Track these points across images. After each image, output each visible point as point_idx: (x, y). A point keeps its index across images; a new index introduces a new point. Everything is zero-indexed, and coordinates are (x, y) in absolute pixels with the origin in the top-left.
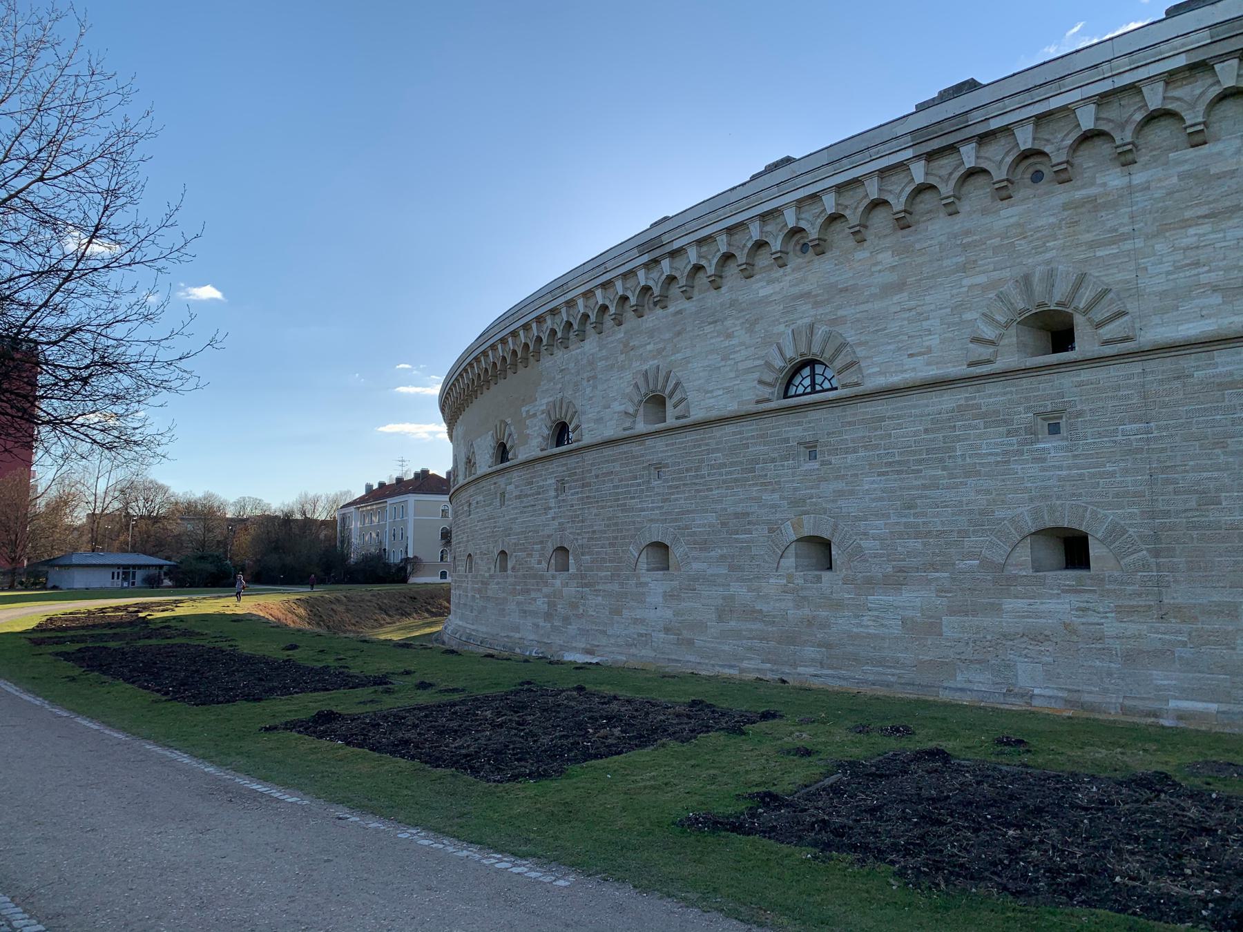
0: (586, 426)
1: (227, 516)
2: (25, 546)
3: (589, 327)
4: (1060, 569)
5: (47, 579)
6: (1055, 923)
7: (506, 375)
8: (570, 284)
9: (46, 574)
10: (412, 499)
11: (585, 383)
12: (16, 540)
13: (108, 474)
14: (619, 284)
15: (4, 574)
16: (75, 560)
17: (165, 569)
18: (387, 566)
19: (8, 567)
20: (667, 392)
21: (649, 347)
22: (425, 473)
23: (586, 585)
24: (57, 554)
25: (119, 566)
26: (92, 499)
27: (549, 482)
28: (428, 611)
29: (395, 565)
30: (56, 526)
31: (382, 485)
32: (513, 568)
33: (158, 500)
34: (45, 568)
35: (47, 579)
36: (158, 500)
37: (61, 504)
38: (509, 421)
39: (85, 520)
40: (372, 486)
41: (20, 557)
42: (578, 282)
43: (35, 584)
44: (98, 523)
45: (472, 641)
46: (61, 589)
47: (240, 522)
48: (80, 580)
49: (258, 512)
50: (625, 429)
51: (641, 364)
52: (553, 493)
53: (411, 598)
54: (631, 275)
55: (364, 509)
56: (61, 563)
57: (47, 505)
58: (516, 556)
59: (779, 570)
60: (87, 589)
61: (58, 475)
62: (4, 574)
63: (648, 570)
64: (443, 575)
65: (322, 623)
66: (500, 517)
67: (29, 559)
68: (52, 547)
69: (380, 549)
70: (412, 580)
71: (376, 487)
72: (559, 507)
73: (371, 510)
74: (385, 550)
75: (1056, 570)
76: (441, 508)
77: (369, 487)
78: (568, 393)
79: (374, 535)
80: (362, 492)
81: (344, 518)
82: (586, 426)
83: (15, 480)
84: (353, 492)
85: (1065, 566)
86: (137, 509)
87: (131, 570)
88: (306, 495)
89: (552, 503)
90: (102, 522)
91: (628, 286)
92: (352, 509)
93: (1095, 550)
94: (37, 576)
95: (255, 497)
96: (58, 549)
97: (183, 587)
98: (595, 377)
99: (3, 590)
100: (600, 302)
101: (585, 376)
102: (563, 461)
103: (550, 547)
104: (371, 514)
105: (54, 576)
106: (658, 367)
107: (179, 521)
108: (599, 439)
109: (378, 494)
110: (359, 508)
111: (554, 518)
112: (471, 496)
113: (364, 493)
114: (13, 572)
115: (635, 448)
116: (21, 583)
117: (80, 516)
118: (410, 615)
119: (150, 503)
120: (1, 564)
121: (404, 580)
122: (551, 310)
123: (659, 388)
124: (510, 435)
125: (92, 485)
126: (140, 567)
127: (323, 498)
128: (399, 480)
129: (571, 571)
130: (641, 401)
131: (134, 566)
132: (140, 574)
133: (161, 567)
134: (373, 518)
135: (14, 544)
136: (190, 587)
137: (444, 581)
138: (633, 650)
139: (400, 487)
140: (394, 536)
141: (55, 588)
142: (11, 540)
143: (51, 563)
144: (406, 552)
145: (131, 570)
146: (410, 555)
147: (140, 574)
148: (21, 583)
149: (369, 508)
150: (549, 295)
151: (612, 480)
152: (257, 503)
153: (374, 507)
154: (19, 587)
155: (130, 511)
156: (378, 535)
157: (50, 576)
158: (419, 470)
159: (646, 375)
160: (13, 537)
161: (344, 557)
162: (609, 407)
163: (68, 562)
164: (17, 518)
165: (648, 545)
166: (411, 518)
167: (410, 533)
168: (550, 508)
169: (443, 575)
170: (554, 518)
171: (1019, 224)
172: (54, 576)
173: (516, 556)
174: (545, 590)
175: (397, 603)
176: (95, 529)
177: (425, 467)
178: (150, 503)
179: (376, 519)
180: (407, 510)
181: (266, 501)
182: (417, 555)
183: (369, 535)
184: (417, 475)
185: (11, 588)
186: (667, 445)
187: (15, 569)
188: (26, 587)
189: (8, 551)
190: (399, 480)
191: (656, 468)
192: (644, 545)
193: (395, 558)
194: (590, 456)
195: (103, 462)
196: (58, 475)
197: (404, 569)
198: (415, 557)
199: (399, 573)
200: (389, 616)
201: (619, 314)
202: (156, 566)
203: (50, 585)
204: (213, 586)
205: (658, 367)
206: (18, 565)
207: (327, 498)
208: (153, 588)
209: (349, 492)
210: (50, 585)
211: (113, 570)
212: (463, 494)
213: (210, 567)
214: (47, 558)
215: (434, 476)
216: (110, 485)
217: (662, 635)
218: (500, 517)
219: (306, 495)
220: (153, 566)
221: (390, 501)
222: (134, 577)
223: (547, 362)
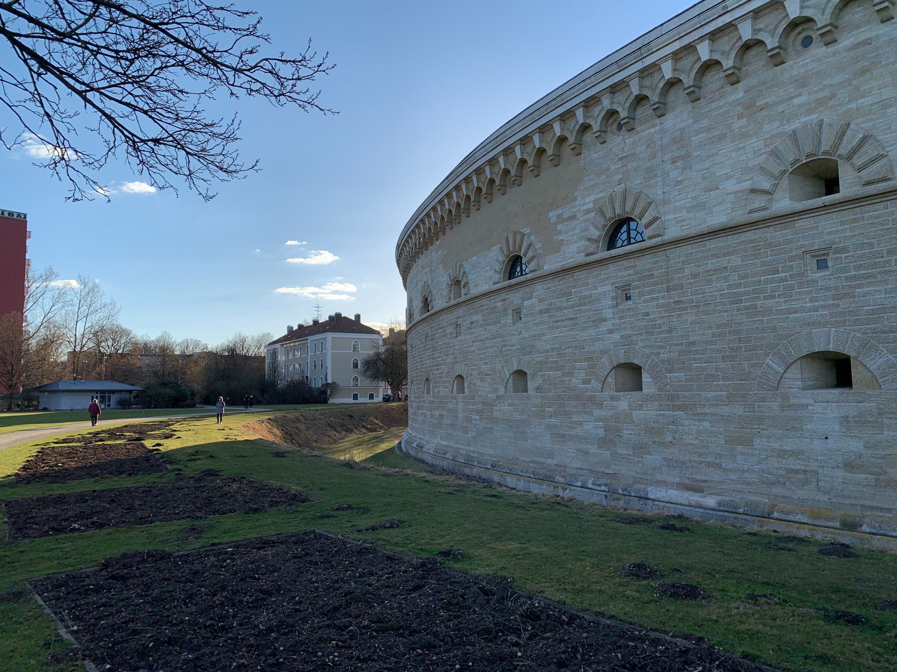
0: (671, 217)
1: (176, 353)
2: (20, 376)
3: (495, 189)
4: (828, 386)
5: (39, 402)
6: (13, 377)
7: (521, 181)
8: (653, 44)
9: (37, 399)
10: (330, 336)
11: (668, 166)
12: (12, 370)
13: (85, 319)
14: (536, 138)
15: (3, 398)
16: (61, 387)
17: (134, 394)
18: (311, 389)
19: (6, 392)
20: (522, 252)
21: (797, 101)
22: (338, 315)
23: (679, 408)
24: (46, 382)
25: (97, 391)
26: (73, 339)
27: (604, 289)
28: (364, 427)
29: (318, 389)
30: (44, 359)
31: (301, 327)
32: (538, 389)
33: (123, 341)
34: (36, 394)
35: (39, 402)
36: (123, 341)
37: (48, 343)
38: (527, 230)
39: (66, 357)
40: (292, 328)
41: (16, 384)
42: (669, 39)
43: (28, 406)
44: (78, 357)
45: (476, 463)
46: (50, 411)
47: (185, 357)
48: (65, 403)
49: (198, 351)
50: (495, 284)
51: (782, 125)
52: (609, 302)
53: (349, 416)
54: (732, 29)
55: (288, 345)
56: (49, 389)
57: (38, 343)
58: (541, 376)
59: (780, 388)
60: (72, 410)
61: (45, 320)
62: (3, 398)
63: (803, 389)
64: (355, 397)
65: (294, 441)
66: (514, 335)
67: (23, 386)
68: (42, 375)
69: (303, 377)
70: (331, 401)
71: (295, 328)
72: (621, 318)
73: (294, 346)
74: (307, 377)
75: (822, 388)
76: (353, 344)
77: (290, 329)
78: (636, 183)
79: (297, 366)
80: (285, 333)
81: (274, 354)
82: (671, 217)
83: (10, 322)
84: (272, 334)
85: (835, 382)
86: (107, 348)
87: (107, 394)
88: (240, 336)
89: (608, 313)
90: (81, 356)
91: (761, 26)
92: (278, 345)
93: (646, 378)
94: (30, 400)
95: (195, 339)
96: (48, 378)
97: (150, 408)
98: (688, 155)
99: (2, 412)
100: (538, 146)
101: (667, 157)
102: (631, 263)
103: (606, 364)
104: (294, 349)
105: (44, 399)
106: (820, 124)
107: (139, 357)
108: (704, 228)
109: (298, 334)
110: (283, 345)
111: (611, 332)
112: (458, 318)
113: (286, 333)
114: (11, 397)
115: (773, 234)
116: (18, 406)
117: (62, 354)
118: (352, 431)
119: (117, 343)
120: (2, 391)
121: (325, 401)
122: (489, 161)
123: (517, 249)
124: (530, 245)
125: (73, 327)
126: (114, 392)
127: (249, 338)
128: (301, 327)
129: (645, 390)
130: (785, 172)
131: (109, 392)
132: (114, 398)
133: (131, 392)
134: (296, 353)
135: (11, 374)
136: (156, 407)
137: (371, 401)
138: (777, 490)
139: (317, 328)
140: (315, 366)
141: (45, 409)
142: (8, 371)
143: (41, 389)
144: (326, 379)
145: (107, 394)
146: (329, 381)
147: (114, 398)
148: (18, 406)
149: (292, 344)
150: (615, 66)
151: (725, 278)
152: (197, 344)
153: (297, 343)
154: (17, 409)
155: (102, 350)
156: (300, 366)
157: (41, 400)
158: (333, 314)
159: (794, 136)
160: (10, 368)
161: (273, 384)
162: (717, 189)
163: (54, 389)
164: (13, 352)
165: (803, 357)
166: (329, 351)
167: (329, 364)
168: (605, 320)
169: (355, 397)
170: (611, 332)
171: (405, 271)
172: (44, 399)
173: (541, 376)
174: (597, 413)
175: (341, 421)
176: (76, 363)
177: (338, 311)
178: (117, 343)
179: (298, 354)
180: (326, 345)
181: (204, 342)
182: (335, 381)
183: (292, 366)
184: (331, 318)
185: (9, 410)
186: (842, 223)
187: (12, 394)
188: (21, 409)
189: (6, 379)
190: (316, 322)
191: (624, 290)
192: (796, 356)
193: (316, 384)
194: (678, 254)
195: (81, 309)
196: (45, 320)
197: (325, 392)
198: (334, 383)
199: (321, 396)
200: (338, 432)
201: (503, 186)
202: (127, 391)
203: (41, 408)
204: (173, 407)
205: (820, 124)
206: (15, 391)
207: (253, 338)
208: (125, 409)
209: (264, 335)
210: (41, 408)
211: (92, 394)
212: (445, 316)
213: (169, 391)
214: (38, 385)
215: (345, 318)
216: (86, 327)
217: (841, 474)
218: (514, 335)
219: (240, 336)
220: (124, 391)
221: (311, 338)
222: (109, 401)
223: (594, 153)
